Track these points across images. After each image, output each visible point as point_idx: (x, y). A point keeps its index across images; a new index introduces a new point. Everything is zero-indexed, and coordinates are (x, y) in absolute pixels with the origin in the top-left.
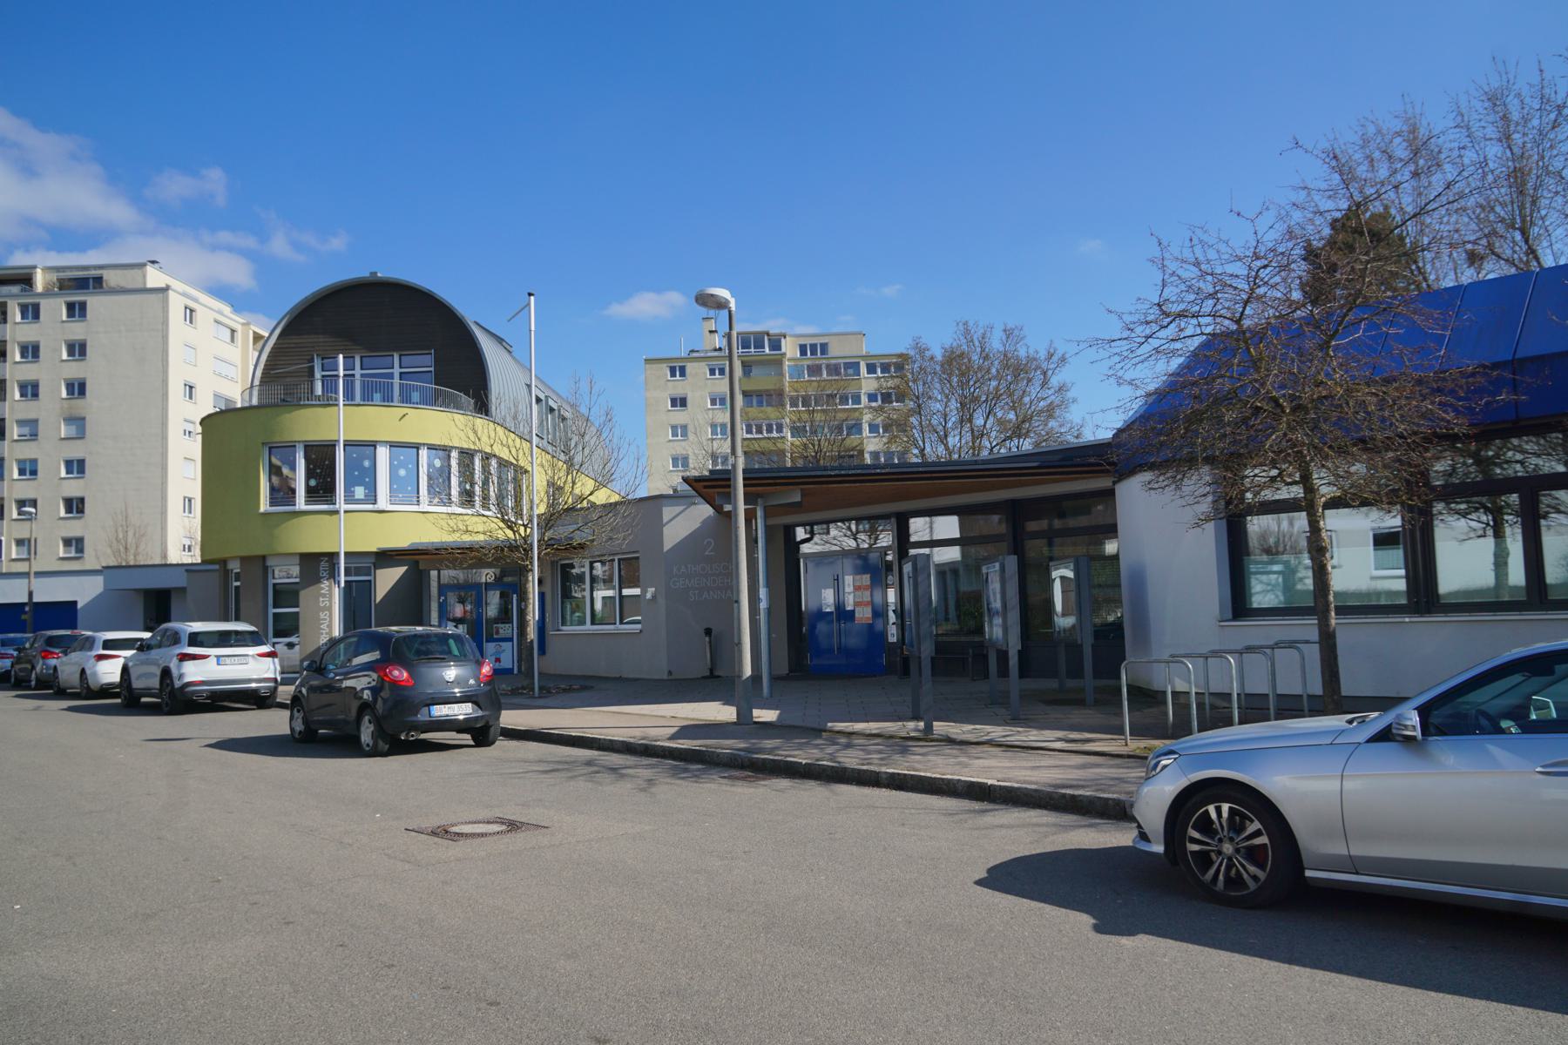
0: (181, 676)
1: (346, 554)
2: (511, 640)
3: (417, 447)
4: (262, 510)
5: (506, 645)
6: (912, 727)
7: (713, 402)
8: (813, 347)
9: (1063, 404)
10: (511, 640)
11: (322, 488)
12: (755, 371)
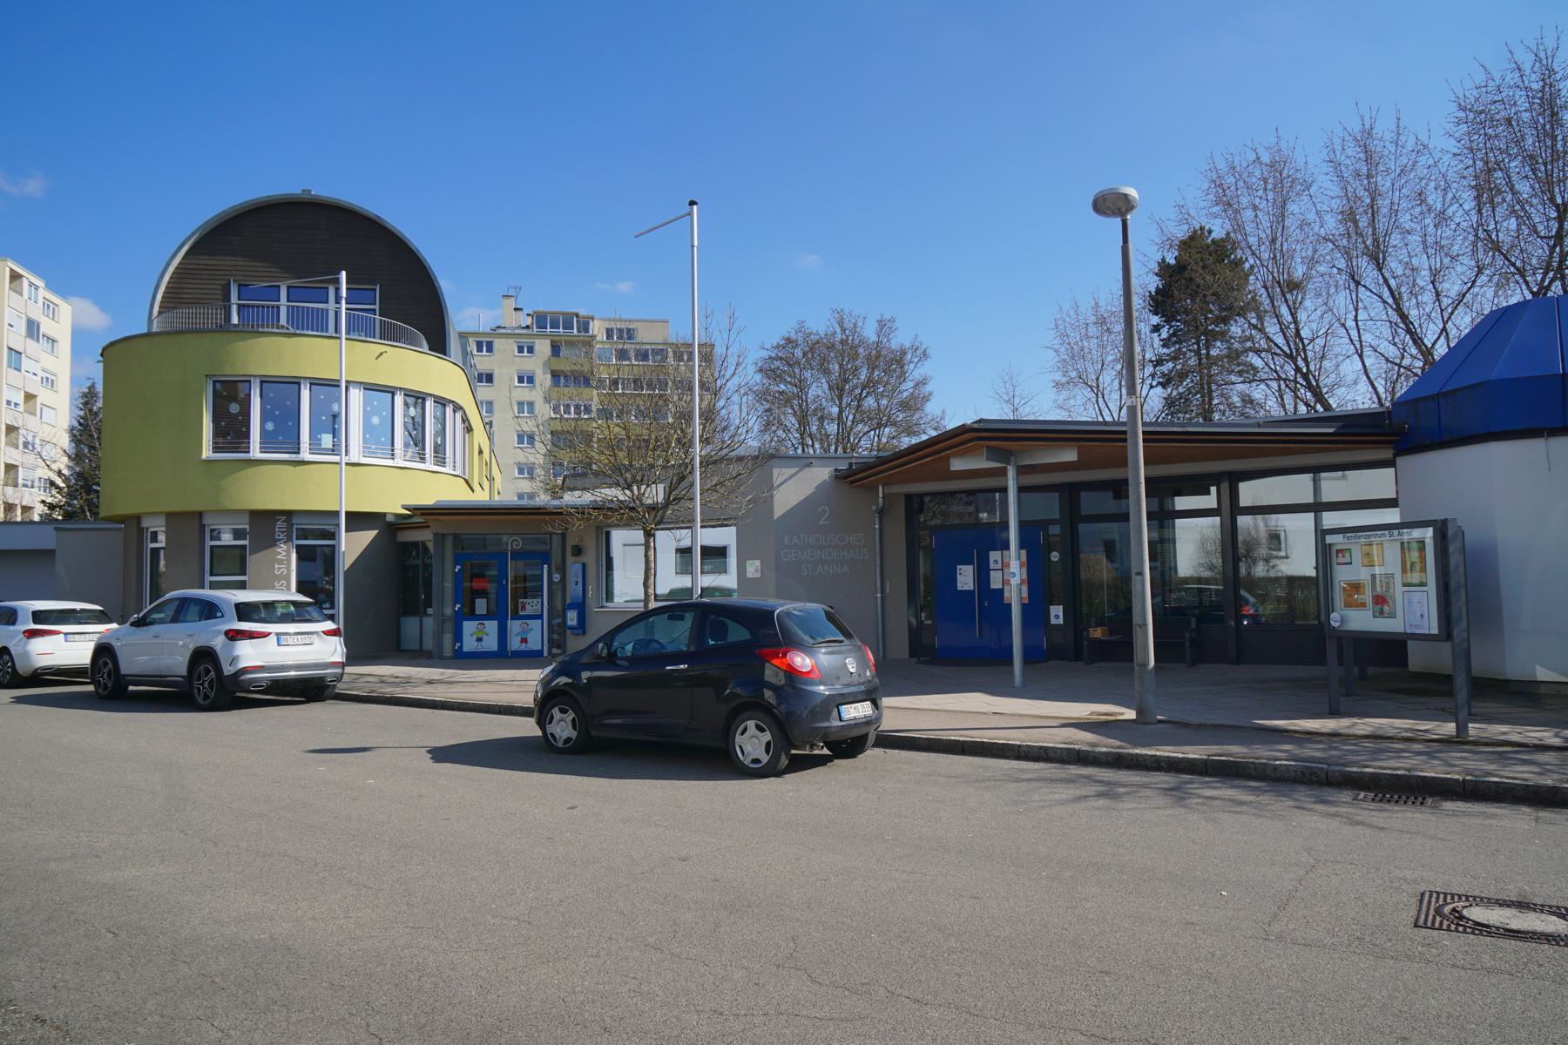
0: (234, 660)
1: (347, 513)
2: (540, 617)
3: (392, 391)
4: (204, 456)
5: (534, 624)
6: (1450, 728)
7: (521, 380)
8: (620, 330)
9: (926, 399)
10: (540, 617)
11: (284, 435)
12: (564, 351)
